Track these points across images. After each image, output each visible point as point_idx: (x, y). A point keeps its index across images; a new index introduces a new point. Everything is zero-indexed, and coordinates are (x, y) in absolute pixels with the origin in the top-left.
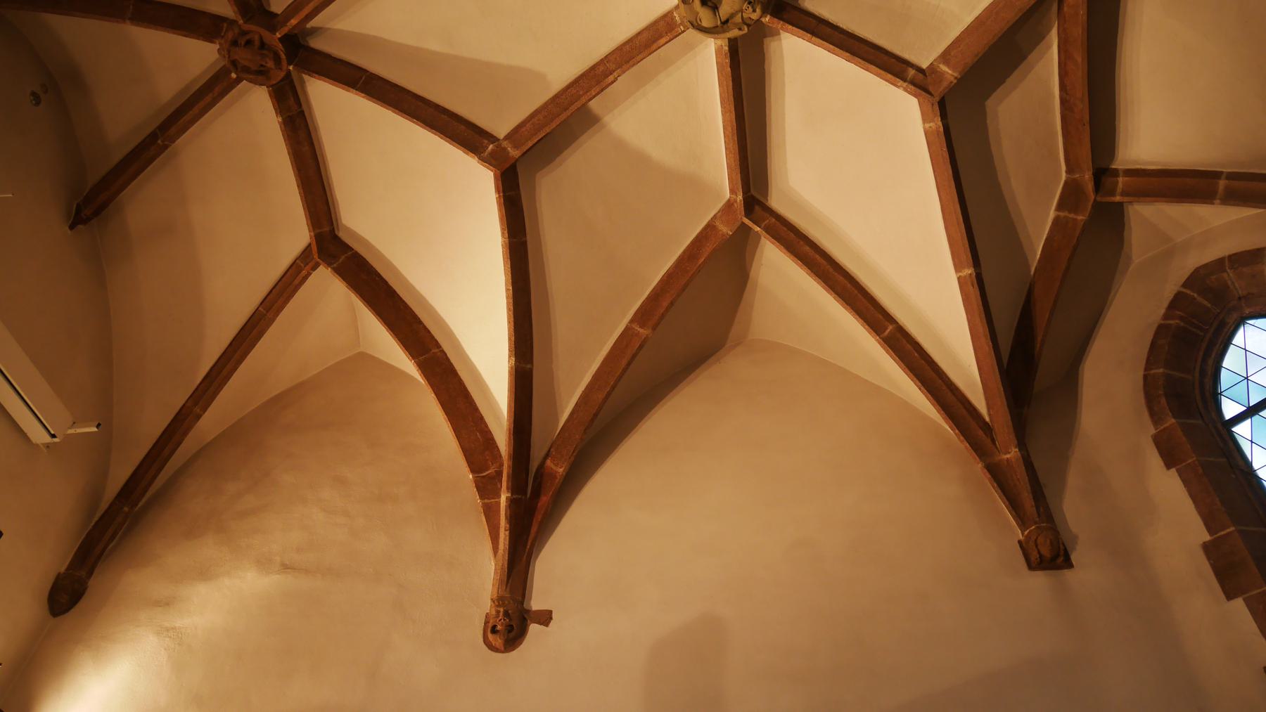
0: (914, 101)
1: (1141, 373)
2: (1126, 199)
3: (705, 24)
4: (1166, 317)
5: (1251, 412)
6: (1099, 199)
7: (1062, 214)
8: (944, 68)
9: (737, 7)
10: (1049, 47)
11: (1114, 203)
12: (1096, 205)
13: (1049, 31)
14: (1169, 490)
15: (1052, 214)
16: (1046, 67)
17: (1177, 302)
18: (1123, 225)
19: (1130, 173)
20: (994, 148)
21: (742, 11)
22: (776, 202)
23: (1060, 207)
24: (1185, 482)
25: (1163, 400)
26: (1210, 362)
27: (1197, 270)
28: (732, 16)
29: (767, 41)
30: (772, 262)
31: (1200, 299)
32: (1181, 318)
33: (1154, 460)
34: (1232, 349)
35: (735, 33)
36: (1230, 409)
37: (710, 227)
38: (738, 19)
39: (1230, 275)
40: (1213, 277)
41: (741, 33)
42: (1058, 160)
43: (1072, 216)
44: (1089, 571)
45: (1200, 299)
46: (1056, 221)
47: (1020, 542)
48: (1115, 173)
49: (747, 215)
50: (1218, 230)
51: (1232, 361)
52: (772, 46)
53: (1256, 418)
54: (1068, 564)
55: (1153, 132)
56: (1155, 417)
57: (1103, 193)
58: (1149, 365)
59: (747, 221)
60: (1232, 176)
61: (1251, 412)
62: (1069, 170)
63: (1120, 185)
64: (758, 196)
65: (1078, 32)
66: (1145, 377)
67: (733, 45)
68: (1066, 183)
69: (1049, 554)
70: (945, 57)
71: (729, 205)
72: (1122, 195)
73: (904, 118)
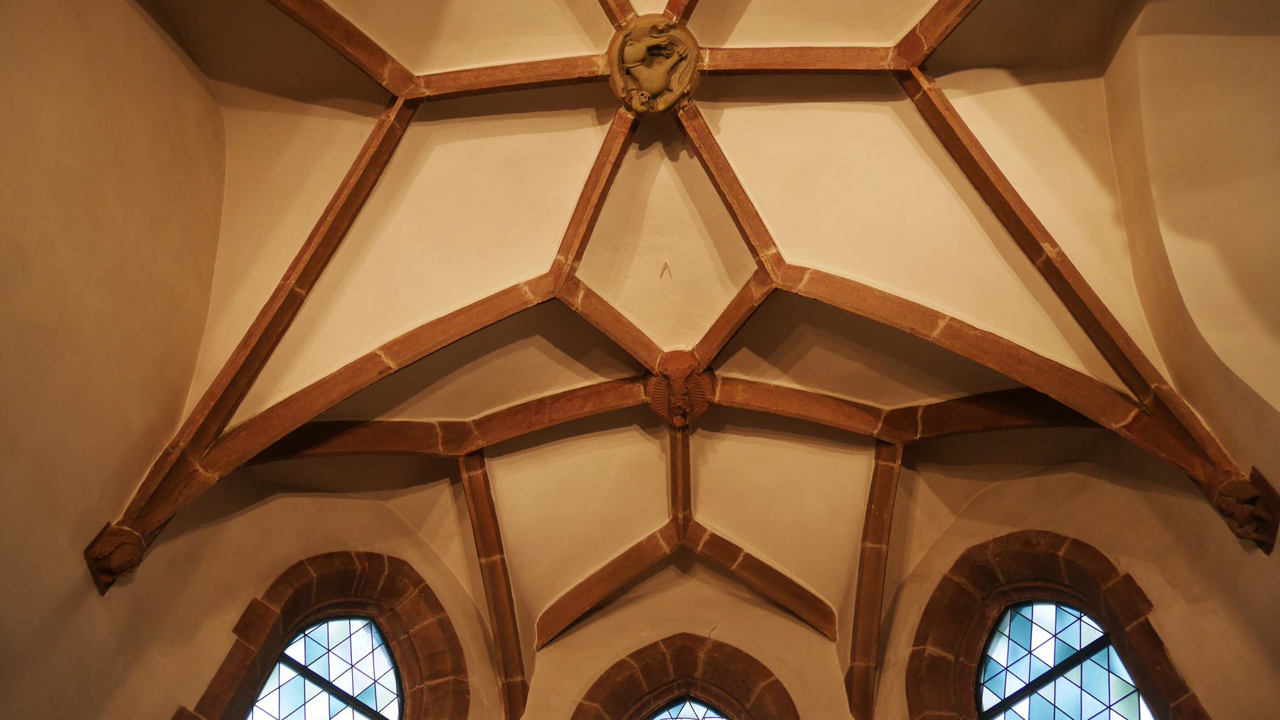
0: (545, 268)
1: (303, 557)
2: (466, 484)
3: (628, 49)
4: (359, 555)
5: (304, 671)
6: (461, 459)
7: (438, 430)
8: (581, 294)
9: (646, 85)
10: (587, 378)
11: (459, 472)
12: (455, 460)
13: (602, 375)
14: (216, 642)
15: (434, 420)
16: (576, 379)
17: (374, 558)
18: (426, 482)
19: (485, 475)
20: (494, 354)
21: (640, 89)
22: (415, 131)
23: (444, 425)
24: (231, 656)
25: (290, 592)
26: (329, 611)
27: (405, 563)
28: (636, 80)
29: (593, 112)
30: (343, 138)
31: (384, 577)
32: (363, 569)
33: (233, 614)
34: (346, 622)
35: (619, 82)
36: (295, 651)
37: (383, 57)
38: (632, 86)
39: (413, 593)
40: (406, 580)
41: (620, 91)
42: (484, 410)
43: (440, 440)
44: (103, 614)
45: (384, 577)
46: (429, 427)
47: (109, 524)
48: (483, 465)
49: (406, 102)
50: (447, 564)
51: (336, 628)
52: (588, 116)
53: (300, 679)
54: (103, 588)
55: (520, 484)
56: (273, 592)
57: (454, 461)
58: (313, 560)
59: (400, 102)
60: (503, 560)
61: (304, 671)
62: (478, 423)
63: (475, 473)
64: (419, 109)
65: (611, 402)
66: (301, 563)
67: (605, 79)
68: (464, 423)
69: (107, 565)
70: (590, 294)
71: (410, 78)
72: (470, 478)
73: (526, 263)
